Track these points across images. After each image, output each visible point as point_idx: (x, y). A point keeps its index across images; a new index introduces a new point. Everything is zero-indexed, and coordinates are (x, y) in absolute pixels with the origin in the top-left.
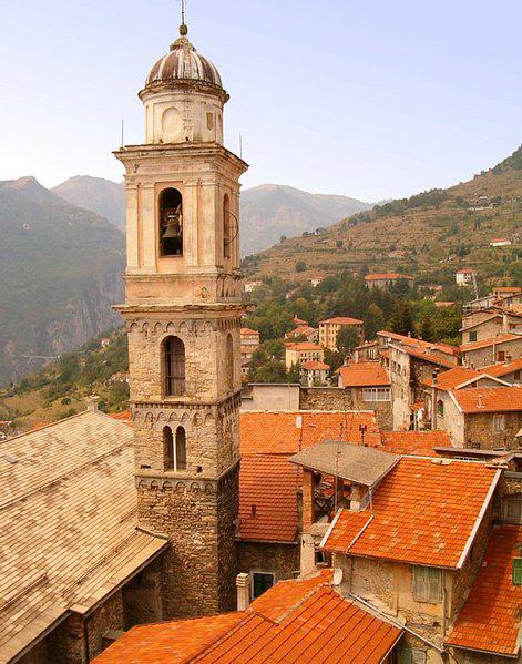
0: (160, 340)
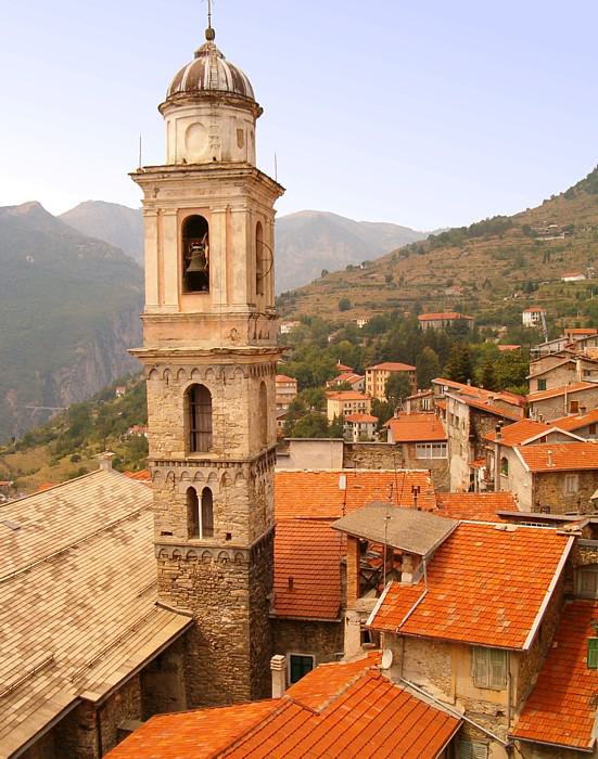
0: (184, 388)
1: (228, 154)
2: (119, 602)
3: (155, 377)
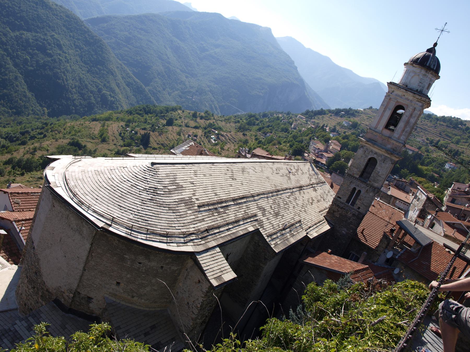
0: (369, 157)
1: (423, 90)
2: (315, 210)
3: (362, 149)
